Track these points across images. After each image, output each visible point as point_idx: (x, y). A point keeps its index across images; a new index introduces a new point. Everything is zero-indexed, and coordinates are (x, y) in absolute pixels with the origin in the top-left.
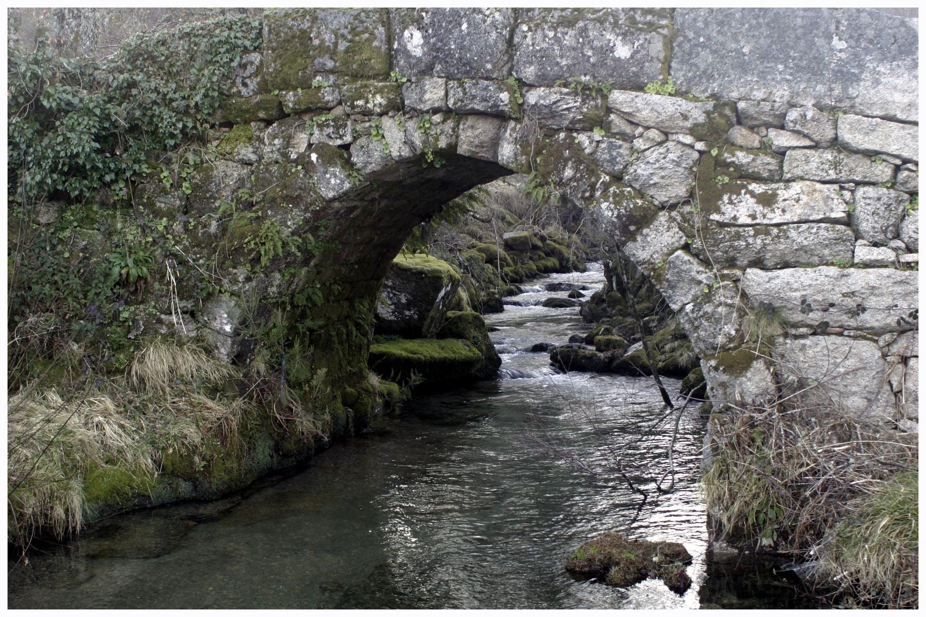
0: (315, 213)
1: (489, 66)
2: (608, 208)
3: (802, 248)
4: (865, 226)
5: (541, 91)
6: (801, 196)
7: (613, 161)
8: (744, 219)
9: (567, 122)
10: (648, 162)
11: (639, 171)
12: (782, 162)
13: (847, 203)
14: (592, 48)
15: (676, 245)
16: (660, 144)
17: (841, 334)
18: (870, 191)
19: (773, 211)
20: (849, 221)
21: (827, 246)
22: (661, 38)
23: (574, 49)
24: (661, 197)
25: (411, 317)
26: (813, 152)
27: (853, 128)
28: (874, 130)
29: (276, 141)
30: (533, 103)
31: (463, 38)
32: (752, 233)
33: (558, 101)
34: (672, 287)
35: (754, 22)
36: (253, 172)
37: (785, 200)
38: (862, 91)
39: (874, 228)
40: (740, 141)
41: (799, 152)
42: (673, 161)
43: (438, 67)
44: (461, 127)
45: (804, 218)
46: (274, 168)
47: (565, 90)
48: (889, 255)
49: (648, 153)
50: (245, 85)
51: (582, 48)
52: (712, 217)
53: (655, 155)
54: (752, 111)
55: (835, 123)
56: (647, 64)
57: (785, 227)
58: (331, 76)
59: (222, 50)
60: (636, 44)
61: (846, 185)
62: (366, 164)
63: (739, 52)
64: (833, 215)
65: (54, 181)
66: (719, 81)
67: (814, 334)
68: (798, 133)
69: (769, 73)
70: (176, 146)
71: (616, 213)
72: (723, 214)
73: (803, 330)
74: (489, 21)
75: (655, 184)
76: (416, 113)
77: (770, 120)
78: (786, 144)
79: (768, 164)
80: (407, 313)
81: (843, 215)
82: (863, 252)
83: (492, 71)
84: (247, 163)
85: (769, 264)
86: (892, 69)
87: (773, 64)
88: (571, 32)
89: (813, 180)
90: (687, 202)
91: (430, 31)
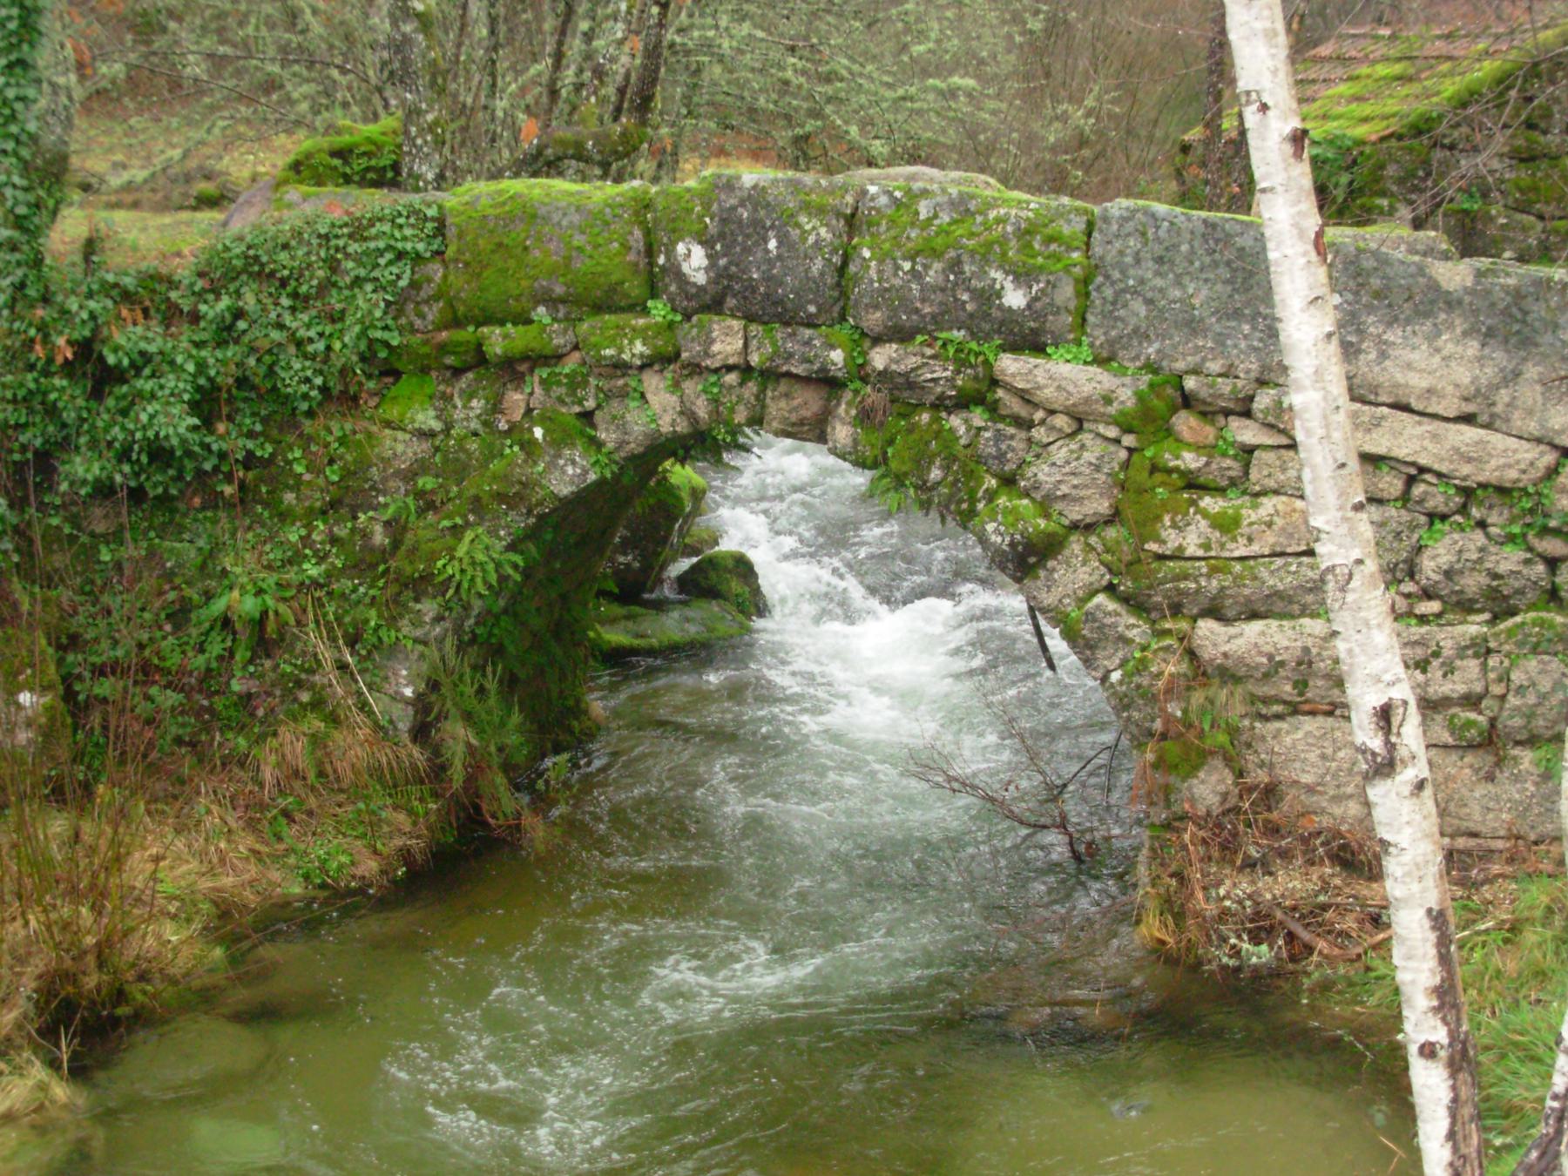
0: (541, 517)
2: (997, 531)
3: (1277, 594)
6: (1275, 519)
7: (1001, 457)
8: (1191, 550)
9: (933, 398)
10: (1054, 464)
11: (1041, 477)
14: (968, 289)
15: (1096, 586)
17: (1330, 713)
19: (1234, 539)
22: (1072, 282)
23: (943, 290)
24: (1075, 513)
25: (628, 565)
28: (1378, 425)
29: (474, 403)
32: (1204, 570)
35: (1207, 260)
37: (1251, 524)
40: (1187, 435)
42: (1091, 464)
43: (731, 302)
44: (769, 393)
45: (1278, 549)
46: (473, 445)
47: (929, 352)
49: (1053, 448)
50: (423, 317)
51: (953, 290)
52: (1146, 546)
53: (1064, 452)
54: (1204, 393)
57: (1252, 563)
58: (561, 307)
59: (382, 261)
60: (1035, 288)
62: (621, 444)
63: (1186, 302)
66: (1156, 345)
68: (1271, 426)
71: (1008, 539)
72: (1164, 542)
73: (1277, 708)
74: (811, 239)
75: (1064, 496)
77: (1231, 405)
79: (1229, 469)
80: (622, 559)
83: (815, 316)
85: (1231, 613)
86: (1404, 338)
87: (1233, 324)
88: (937, 266)
90: (1109, 521)
91: (718, 247)
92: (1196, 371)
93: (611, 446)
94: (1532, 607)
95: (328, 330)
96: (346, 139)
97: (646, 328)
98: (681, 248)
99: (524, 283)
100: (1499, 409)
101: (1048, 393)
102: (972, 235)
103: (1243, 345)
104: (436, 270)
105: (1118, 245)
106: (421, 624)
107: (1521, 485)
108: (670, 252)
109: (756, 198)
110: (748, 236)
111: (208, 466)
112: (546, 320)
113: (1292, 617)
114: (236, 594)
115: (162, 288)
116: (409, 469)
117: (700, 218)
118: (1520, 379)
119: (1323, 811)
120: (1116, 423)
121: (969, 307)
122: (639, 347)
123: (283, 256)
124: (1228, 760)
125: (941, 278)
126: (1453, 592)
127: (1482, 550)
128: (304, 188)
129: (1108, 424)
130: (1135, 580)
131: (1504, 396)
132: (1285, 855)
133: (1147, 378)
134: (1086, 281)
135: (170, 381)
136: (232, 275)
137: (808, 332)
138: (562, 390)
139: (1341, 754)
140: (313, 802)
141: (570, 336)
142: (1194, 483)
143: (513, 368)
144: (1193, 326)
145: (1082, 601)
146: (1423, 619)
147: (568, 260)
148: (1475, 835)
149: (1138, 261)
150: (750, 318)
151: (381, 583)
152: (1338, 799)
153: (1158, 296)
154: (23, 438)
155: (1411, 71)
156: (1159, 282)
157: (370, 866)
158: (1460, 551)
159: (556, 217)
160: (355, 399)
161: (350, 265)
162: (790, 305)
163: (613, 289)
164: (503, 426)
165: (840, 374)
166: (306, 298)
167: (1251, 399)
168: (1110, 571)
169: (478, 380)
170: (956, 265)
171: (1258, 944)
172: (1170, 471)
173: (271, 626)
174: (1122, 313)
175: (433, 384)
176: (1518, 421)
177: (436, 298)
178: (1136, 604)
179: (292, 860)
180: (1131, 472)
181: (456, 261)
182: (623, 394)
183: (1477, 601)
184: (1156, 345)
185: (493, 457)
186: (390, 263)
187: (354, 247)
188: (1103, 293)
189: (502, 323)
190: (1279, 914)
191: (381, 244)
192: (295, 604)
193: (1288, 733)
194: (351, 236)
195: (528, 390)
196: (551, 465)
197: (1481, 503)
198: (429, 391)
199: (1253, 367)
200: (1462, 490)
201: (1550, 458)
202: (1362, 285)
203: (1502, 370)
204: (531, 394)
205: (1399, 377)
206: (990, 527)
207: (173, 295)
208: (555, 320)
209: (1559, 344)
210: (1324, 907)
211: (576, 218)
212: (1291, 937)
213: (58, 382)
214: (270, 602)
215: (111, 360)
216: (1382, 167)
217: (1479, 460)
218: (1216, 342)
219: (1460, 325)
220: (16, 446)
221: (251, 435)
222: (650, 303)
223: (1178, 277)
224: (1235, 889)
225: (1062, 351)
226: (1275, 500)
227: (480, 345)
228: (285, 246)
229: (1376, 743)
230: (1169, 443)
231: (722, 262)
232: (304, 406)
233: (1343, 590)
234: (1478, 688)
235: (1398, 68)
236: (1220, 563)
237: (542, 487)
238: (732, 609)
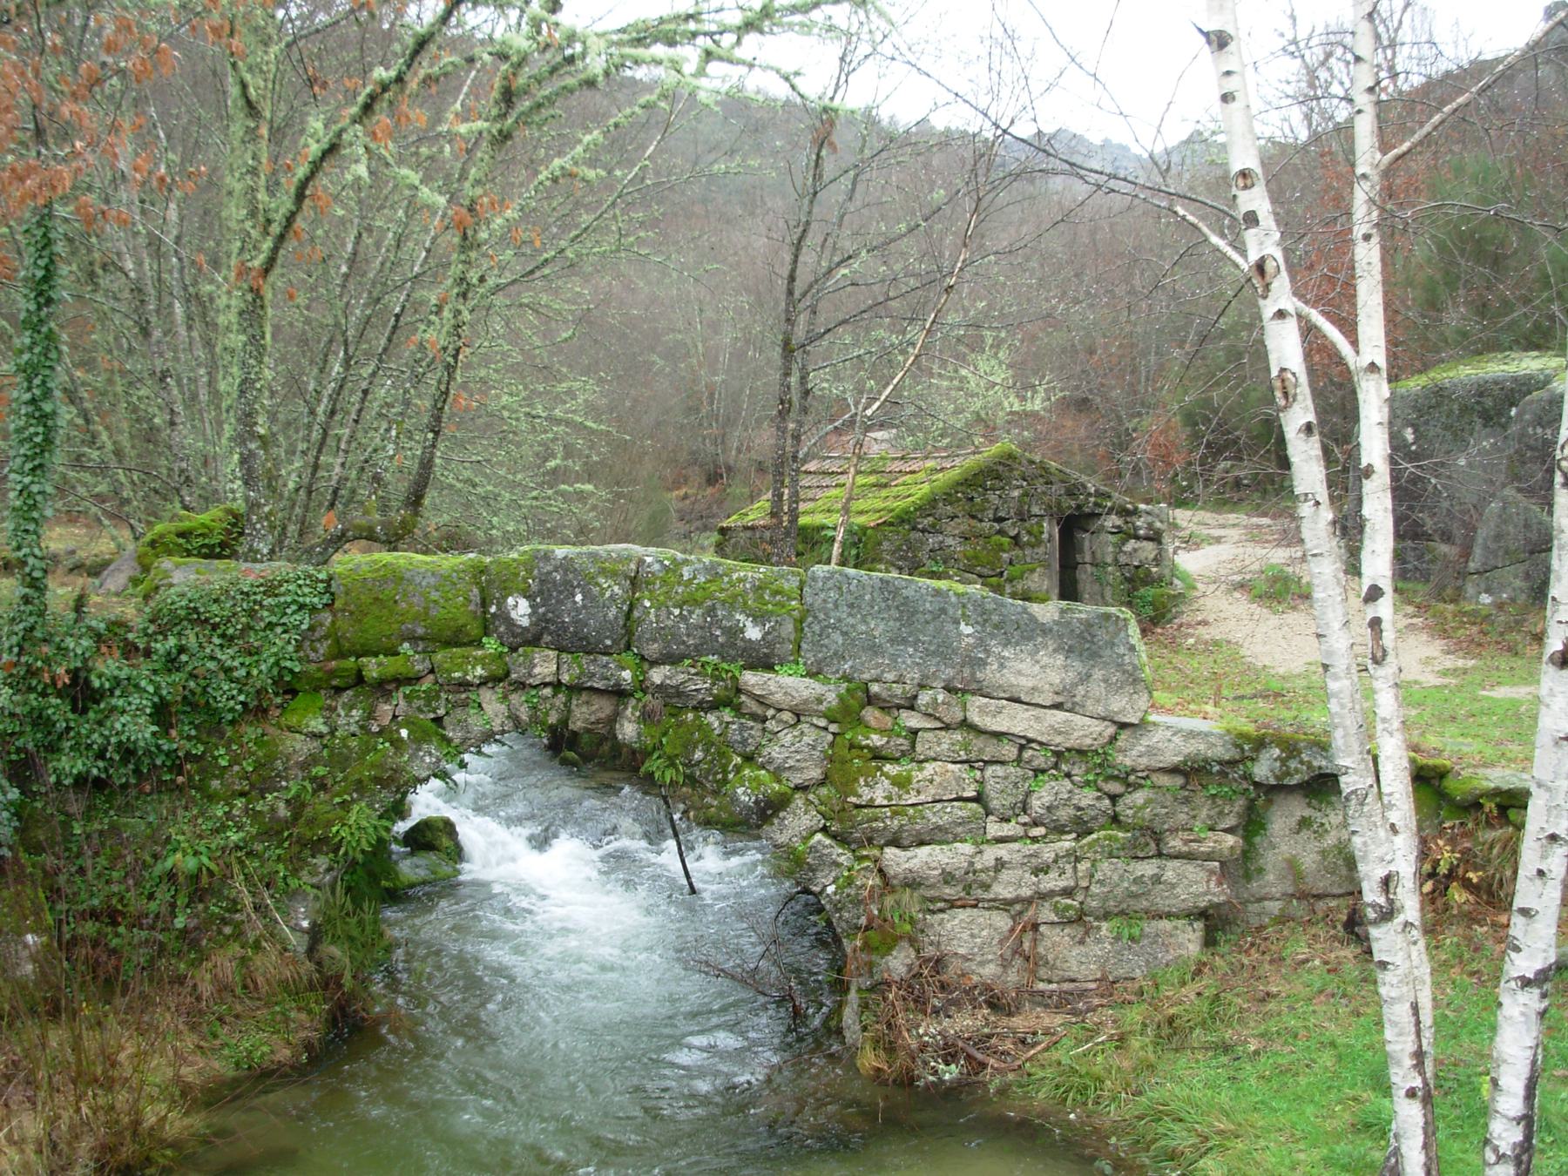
3: (939, 828)
5: (666, 670)
7: (744, 742)
11: (774, 754)
16: (793, 726)
17: (975, 906)
18: (999, 770)
20: (978, 799)
24: (797, 779)
27: (982, 711)
29: (354, 712)
30: (658, 682)
31: (578, 611)
34: (813, 871)
36: (325, 746)
38: (990, 674)
40: (873, 723)
43: (547, 638)
44: (574, 702)
46: (354, 743)
47: (693, 671)
48: (1020, 831)
50: (315, 650)
54: (884, 695)
59: (289, 611)
64: (966, 794)
67: (952, 907)
73: (940, 905)
74: (608, 594)
82: (994, 829)
85: (906, 843)
88: (698, 611)
90: (822, 783)
92: (876, 680)
93: (457, 741)
94: (1102, 828)
95: (248, 660)
96: (187, 524)
97: (484, 658)
98: (510, 601)
99: (395, 626)
100: (1077, 699)
101: (778, 697)
102: (722, 590)
104: (327, 618)
105: (822, 596)
106: (317, 874)
108: (501, 603)
109: (567, 565)
110: (560, 592)
111: (159, 762)
112: (411, 653)
113: (948, 843)
114: (179, 855)
115: (121, 631)
116: (304, 762)
117: (525, 580)
119: (973, 972)
120: (825, 716)
123: (215, 608)
124: (912, 941)
128: (177, 559)
131: (1081, 690)
132: (957, 1003)
135: (135, 700)
136: (175, 621)
137: (605, 658)
138: (422, 702)
139: (984, 933)
140: (239, 1008)
141: (427, 664)
142: (878, 756)
143: (384, 687)
144: (875, 650)
145: (805, 839)
146: (1035, 840)
147: (427, 609)
148: (1073, 981)
149: (836, 606)
150: (561, 649)
151: (286, 844)
152: (982, 964)
154: (20, 743)
155: (884, 481)
156: (851, 621)
157: (285, 1054)
159: (418, 580)
160: (265, 711)
161: (266, 614)
163: (460, 630)
164: (375, 729)
166: (232, 638)
167: (915, 697)
169: (356, 696)
170: (711, 611)
171: (948, 1064)
172: (862, 748)
173: (205, 880)
175: (323, 699)
176: (1090, 707)
177: (326, 637)
178: (841, 839)
179: (226, 1052)
181: (344, 610)
182: (465, 705)
185: (369, 752)
186: (294, 613)
187: (268, 601)
189: (376, 655)
190: (960, 1044)
191: (289, 599)
192: (221, 862)
194: (264, 593)
196: (413, 757)
197: (1067, 761)
198: (319, 704)
201: (1111, 730)
205: (1013, 680)
206: (740, 791)
207: (130, 636)
210: (989, 1036)
211: (432, 581)
212: (969, 1057)
213: (54, 701)
214: (205, 860)
215: (96, 683)
216: (880, 544)
217: (1066, 733)
219: (1051, 645)
220: (13, 749)
221: (189, 738)
222: (485, 640)
223: (864, 616)
224: (929, 1029)
226: (934, 764)
227: (359, 671)
228: (216, 601)
229: (1382, 901)
231: (541, 610)
232: (230, 717)
233: (1362, 804)
235: (872, 479)
238: (444, 856)
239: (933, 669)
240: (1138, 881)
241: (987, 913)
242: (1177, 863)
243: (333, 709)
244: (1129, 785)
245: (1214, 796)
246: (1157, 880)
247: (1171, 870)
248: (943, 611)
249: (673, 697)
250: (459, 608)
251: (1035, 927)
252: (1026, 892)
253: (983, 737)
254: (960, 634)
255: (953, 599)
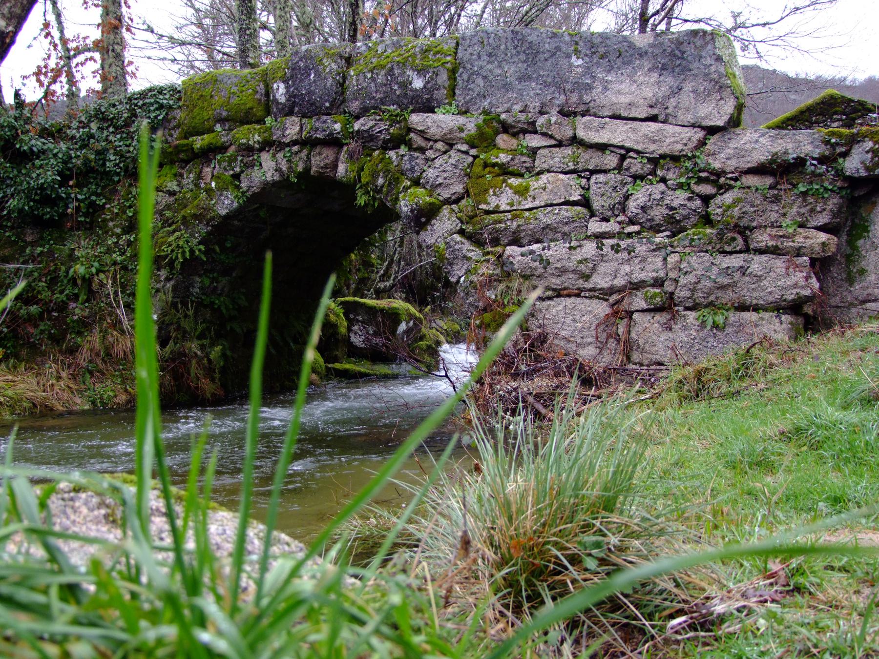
1: (327, 104)
3: (547, 227)
4: (596, 205)
7: (412, 170)
8: (503, 207)
9: (381, 142)
12: (534, 160)
13: (583, 188)
14: (397, 83)
16: (445, 153)
17: (578, 295)
18: (601, 177)
19: (526, 199)
21: (566, 223)
22: (446, 72)
23: (385, 85)
24: (446, 194)
26: (557, 149)
27: (586, 127)
29: (191, 175)
33: (374, 126)
34: (451, 264)
37: (535, 189)
38: (597, 96)
39: (603, 206)
41: (546, 151)
43: (296, 109)
45: (549, 202)
48: (616, 228)
50: (171, 136)
51: (390, 84)
54: (510, 121)
55: (573, 124)
56: (436, 92)
61: (583, 174)
62: (250, 187)
64: (572, 198)
65: (30, 207)
67: (557, 296)
68: (544, 134)
69: (525, 90)
70: (119, 181)
72: (489, 204)
74: (328, 70)
75: (440, 184)
76: (281, 146)
78: (538, 145)
79: (525, 162)
81: (579, 198)
82: (595, 226)
84: (172, 193)
85: (524, 242)
89: (557, 172)
92: (508, 111)
99: (210, 113)
103: (532, 94)
107: (684, 153)
110: (302, 75)
118: (682, 92)
121: (398, 93)
122: (257, 138)
125: (384, 78)
126: (648, 220)
127: (662, 193)
129: (463, 143)
130: (474, 225)
131: (672, 102)
133: (482, 117)
134: (453, 72)
137: (325, 117)
138: (226, 164)
142: (505, 171)
144: (507, 87)
149: (479, 57)
153: (489, 74)
156: (490, 67)
158: (650, 195)
159: (225, 80)
162: (318, 104)
165: (339, 136)
168: (462, 223)
170: (391, 72)
174: (472, 86)
178: (475, 239)
180: (474, 168)
183: (662, 225)
184: (488, 101)
188: (462, 77)
191: (152, 100)
193: (554, 306)
195: (213, 166)
197: (662, 168)
199: (537, 104)
200: (650, 160)
201: (701, 134)
202: (594, 53)
203: (670, 87)
204: (214, 168)
205: (614, 100)
208: (224, 130)
209: (702, 67)
218: (517, 94)
225: (442, 109)
230: (495, 152)
234: (661, 274)
236: (518, 212)
237: (214, 211)
239: (549, 97)
240: (726, 271)
241: (587, 301)
242: (764, 258)
243: (181, 175)
244: (720, 187)
245: (804, 194)
246: (743, 270)
247: (758, 263)
248: (558, 49)
249: (367, 139)
250: (247, 99)
251: (630, 314)
252: (619, 282)
253: (590, 151)
254: (571, 66)
255: (567, 38)
